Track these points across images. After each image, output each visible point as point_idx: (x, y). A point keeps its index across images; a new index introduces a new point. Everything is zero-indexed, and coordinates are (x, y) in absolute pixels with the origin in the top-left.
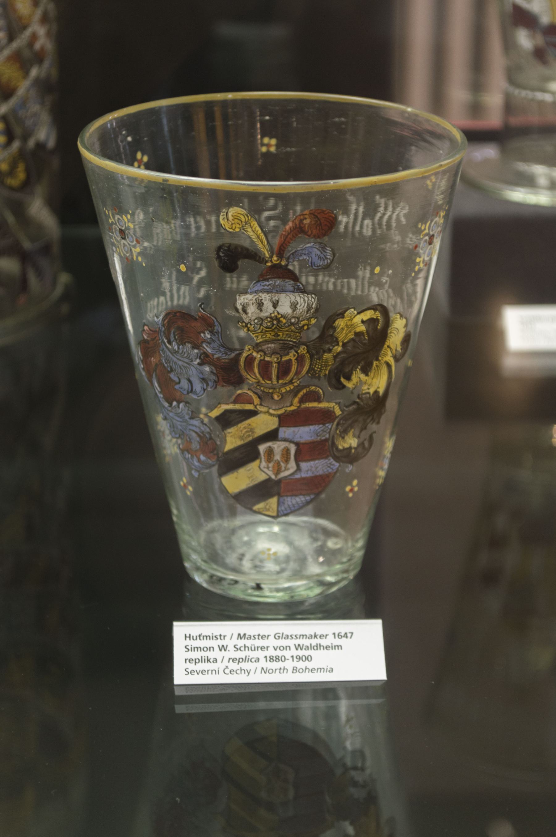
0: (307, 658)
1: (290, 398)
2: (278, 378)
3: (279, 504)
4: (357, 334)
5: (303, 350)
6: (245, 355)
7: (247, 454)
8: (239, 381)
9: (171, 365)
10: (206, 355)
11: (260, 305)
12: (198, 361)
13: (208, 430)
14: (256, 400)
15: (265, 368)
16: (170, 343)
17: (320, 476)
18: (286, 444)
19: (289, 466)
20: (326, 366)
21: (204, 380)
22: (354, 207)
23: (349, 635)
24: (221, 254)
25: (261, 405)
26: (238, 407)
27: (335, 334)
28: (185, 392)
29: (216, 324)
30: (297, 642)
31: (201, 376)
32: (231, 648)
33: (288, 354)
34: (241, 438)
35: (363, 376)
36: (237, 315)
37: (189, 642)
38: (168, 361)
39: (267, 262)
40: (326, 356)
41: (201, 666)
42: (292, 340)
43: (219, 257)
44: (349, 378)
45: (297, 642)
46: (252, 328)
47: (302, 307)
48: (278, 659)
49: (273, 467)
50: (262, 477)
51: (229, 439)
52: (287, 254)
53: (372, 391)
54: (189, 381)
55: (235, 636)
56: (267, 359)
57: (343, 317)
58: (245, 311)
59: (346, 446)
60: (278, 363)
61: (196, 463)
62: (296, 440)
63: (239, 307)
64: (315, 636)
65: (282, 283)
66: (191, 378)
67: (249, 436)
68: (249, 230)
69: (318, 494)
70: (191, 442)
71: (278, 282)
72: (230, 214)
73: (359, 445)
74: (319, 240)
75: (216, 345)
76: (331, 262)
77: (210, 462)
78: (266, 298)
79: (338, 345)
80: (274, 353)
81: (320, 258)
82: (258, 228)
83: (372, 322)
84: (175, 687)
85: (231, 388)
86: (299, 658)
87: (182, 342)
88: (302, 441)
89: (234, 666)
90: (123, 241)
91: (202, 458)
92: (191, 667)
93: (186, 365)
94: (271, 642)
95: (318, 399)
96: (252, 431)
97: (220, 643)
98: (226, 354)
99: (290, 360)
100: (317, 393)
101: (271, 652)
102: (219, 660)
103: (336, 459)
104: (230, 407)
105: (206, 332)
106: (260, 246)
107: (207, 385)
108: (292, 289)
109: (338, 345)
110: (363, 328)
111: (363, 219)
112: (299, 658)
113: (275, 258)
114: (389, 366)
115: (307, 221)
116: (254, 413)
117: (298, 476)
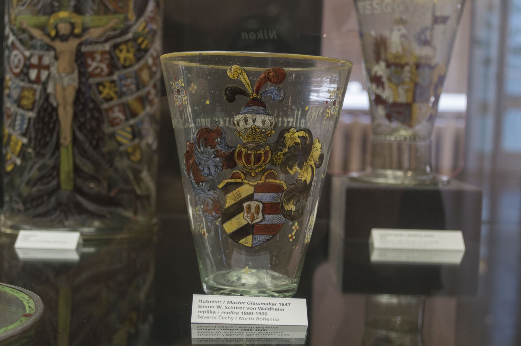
0: (264, 314)
1: (260, 176)
2: (254, 164)
3: (253, 239)
4: (296, 144)
5: (267, 148)
6: (237, 150)
7: (237, 209)
8: (234, 165)
11: (246, 121)
12: (214, 155)
13: (217, 196)
14: (243, 177)
15: (248, 157)
16: (199, 148)
17: (275, 224)
18: (257, 203)
19: (259, 216)
20: (280, 159)
21: (216, 166)
22: (296, 112)
23: (288, 305)
24: (227, 92)
25: (245, 179)
26: (233, 180)
27: (285, 141)
28: (206, 176)
29: (224, 133)
30: (260, 306)
31: (215, 164)
32: (223, 307)
33: (260, 150)
34: (234, 199)
35: (298, 169)
36: (235, 127)
37: (200, 303)
38: (198, 159)
39: (250, 96)
40: (279, 153)
41: (206, 315)
42: (262, 142)
43: (226, 94)
44: (291, 169)
45: (260, 306)
46: (241, 134)
47: (268, 123)
48: (249, 313)
49: (251, 217)
50: (244, 223)
51: (227, 200)
52: (260, 92)
53: (303, 179)
54: (209, 168)
55: (226, 302)
56: (249, 152)
57: (289, 132)
58: (238, 125)
59: (289, 209)
60: (255, 155)
61: (210, 218)
62: (263, 201)
63: (236, 122)
64: (270, 304)
65: (258, 109)
67: (238, 198)
68: (242, 78)
69: (274, 235)
70: (208, 205)
71: (256, 108)
72: (232, 69)
73: (295, 211)
74: (277, 85)
75: (222, 145)
76: (284, 99)
77: (218, 215)
78: (249, 116)
79: (286, 148)
80: (253, 149)
81: (277, 95)
82: (246, 77)
83: (303, 138)
84: (192, 325)
85: (230, 170)
86: (260, 314)
87: (206, 146)
88: (266, 202)
89: (224, 315)
90: (179, 96)
91: (214, 214)
92: (201, 315)
93: (207, 159)
94: (246, 306)
95: (275, 178)
96: (240, 195)
97: (218, 304)
98: (228, 150)
99: (261, 153)
100: (275, 174)
101: (245, 310)
102: (217, 312)
103: (284, 216)
104: (229, 181)
105: (218, 138)
106: (247, 87)
107: (218, 169)
108: (263, 112)
109: (286, 148)
110: (299, 141)
111: (301, 119)
112: (260, 314)
113: (255, 94)
114: (312, 167)
115: (271, 74)
116: (241, 184)
117: (263, 223)
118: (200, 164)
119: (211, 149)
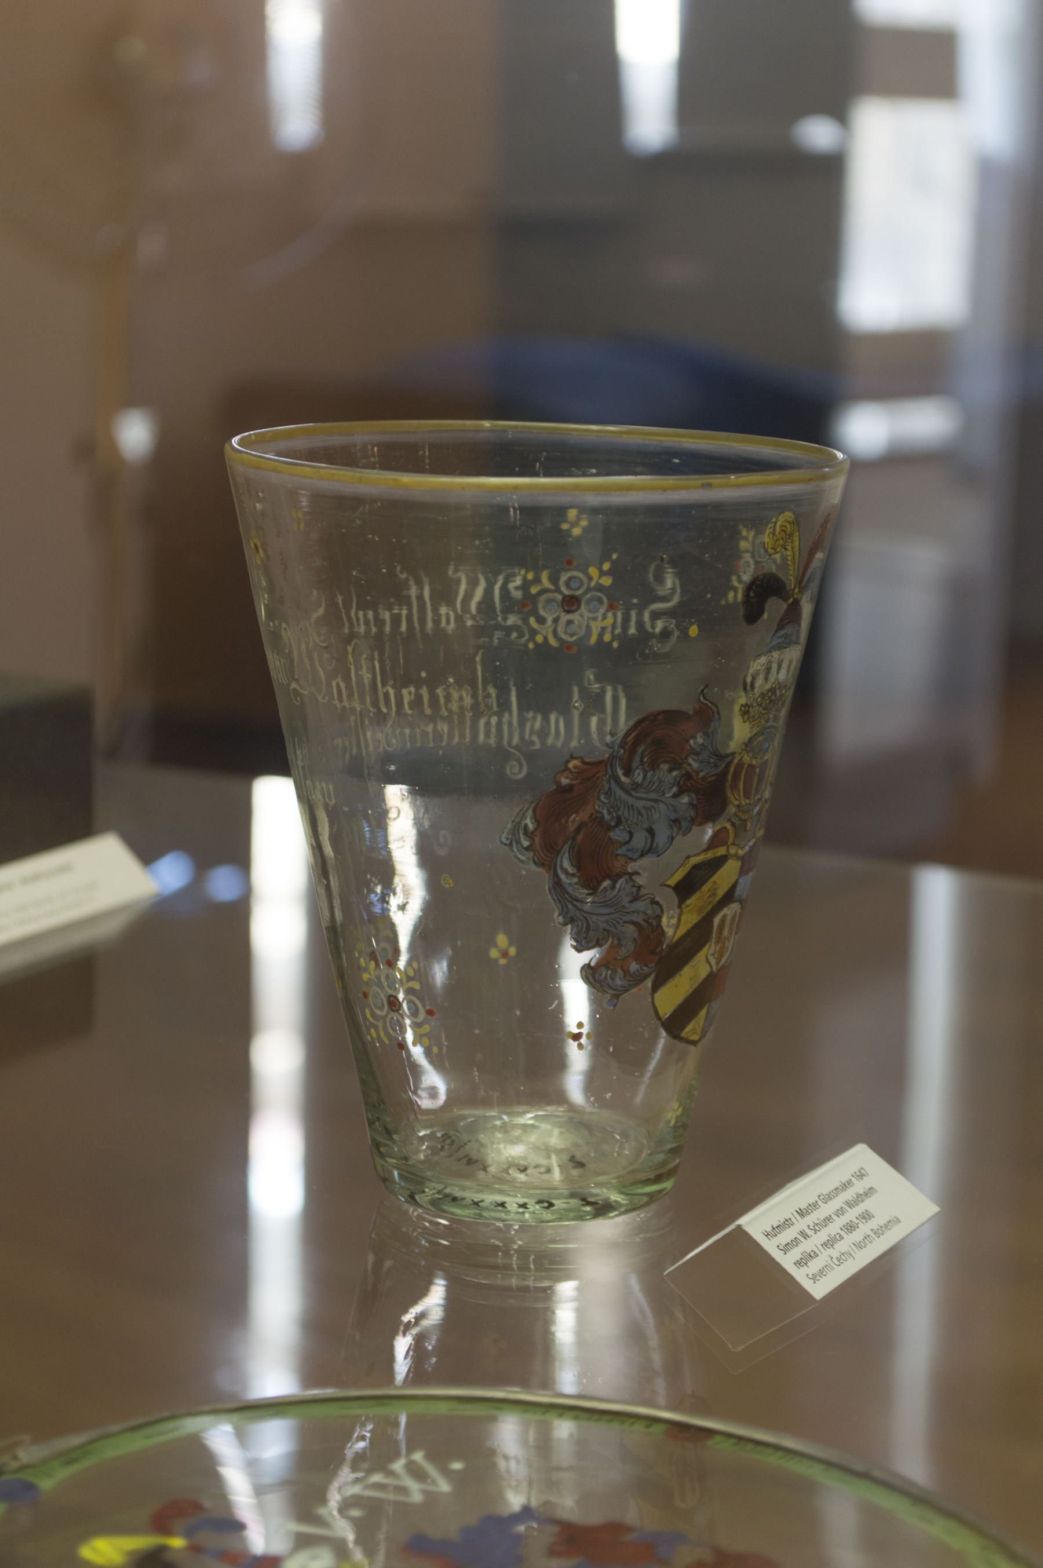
6: (736, 761)
9: (620, 813)
10: (688, 776)
16: (628, 773)
22: (413, 591)
31: (673, 816)
54: (651, 832)
66: (654, 827)
118: (619, 822)
119: (671, 770)
